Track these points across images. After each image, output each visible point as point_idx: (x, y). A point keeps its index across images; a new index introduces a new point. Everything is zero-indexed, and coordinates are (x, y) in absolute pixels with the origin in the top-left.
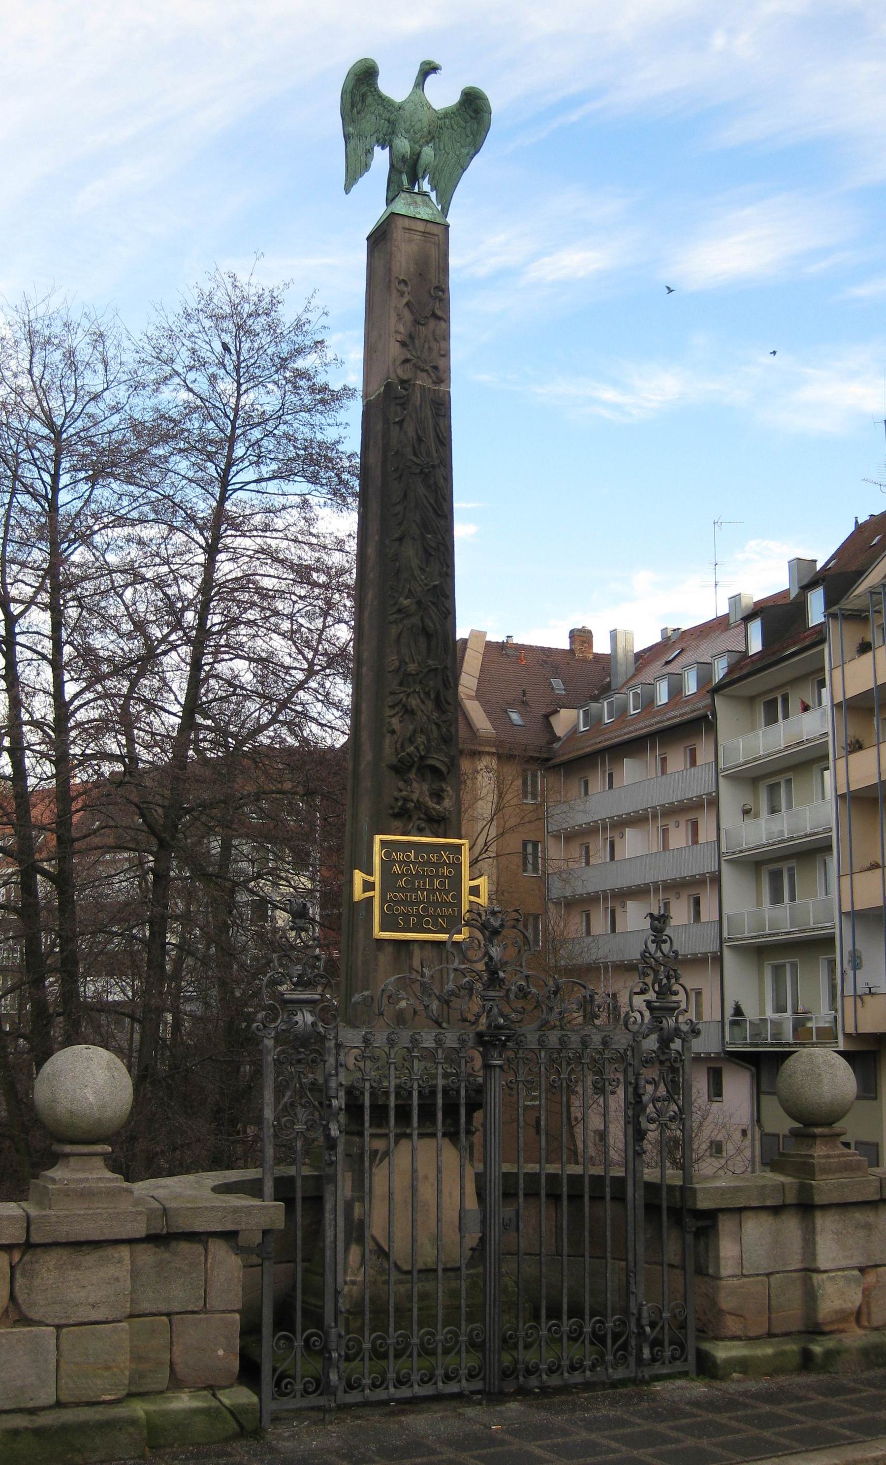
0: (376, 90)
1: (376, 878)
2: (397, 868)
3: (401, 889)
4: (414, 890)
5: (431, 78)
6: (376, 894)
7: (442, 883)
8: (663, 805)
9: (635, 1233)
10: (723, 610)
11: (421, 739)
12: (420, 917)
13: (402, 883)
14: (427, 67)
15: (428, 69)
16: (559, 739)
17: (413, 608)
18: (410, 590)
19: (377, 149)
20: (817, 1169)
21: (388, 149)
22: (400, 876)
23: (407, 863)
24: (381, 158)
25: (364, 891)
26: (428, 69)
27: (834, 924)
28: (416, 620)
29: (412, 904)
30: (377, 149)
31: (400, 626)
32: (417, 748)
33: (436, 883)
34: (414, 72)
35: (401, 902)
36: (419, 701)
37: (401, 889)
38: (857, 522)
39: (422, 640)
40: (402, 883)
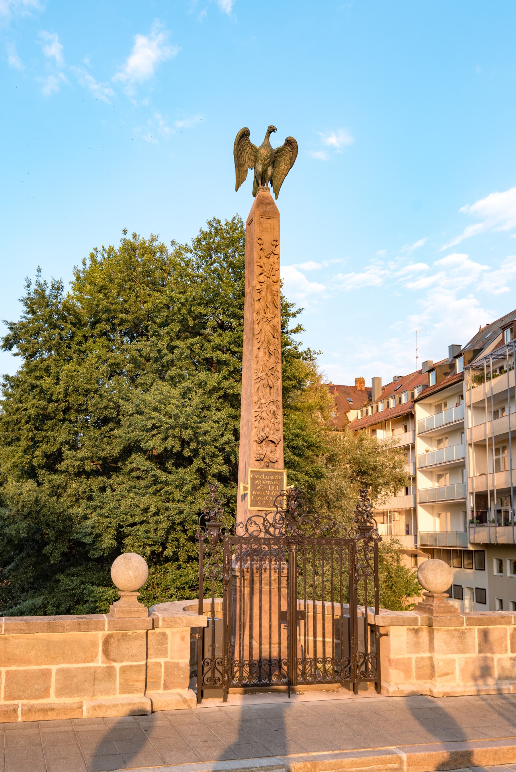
0: (249, 142)
1: (249, 486)
2: (257, 482)
3: (259, 490)
4: (264, 490)
5: (273, 133)
6: (249, 492)
7: (275, 488)
8: (404, 446)
9: (82, 725)
10: (420, 368)
11: (267, 430)
12: (267, 501)
13: (259, 488)
14: (270, 129)
15: (271, 130)
16: (350, 422)
17: (264, 376)
18: (262, 369)
19: (249, 170)
20: (434, 611)
21: (253, 169)
22: (258, 485)
23: (262, 480)
24: (251, 174)
25: (244, 491)
26: (271, 130)
27: (150, 618)
28: (265, 381)
29: (263, 496)
30: (249, 170)
31: (259, 384)
32: (265, 434)
33: (273, 487)
34: (266, 131)
35: (260, 495)
36: (266, 415)
37: (259, 490)
38: (480, 328)
39: (268, 388)
40: (259, 488)
